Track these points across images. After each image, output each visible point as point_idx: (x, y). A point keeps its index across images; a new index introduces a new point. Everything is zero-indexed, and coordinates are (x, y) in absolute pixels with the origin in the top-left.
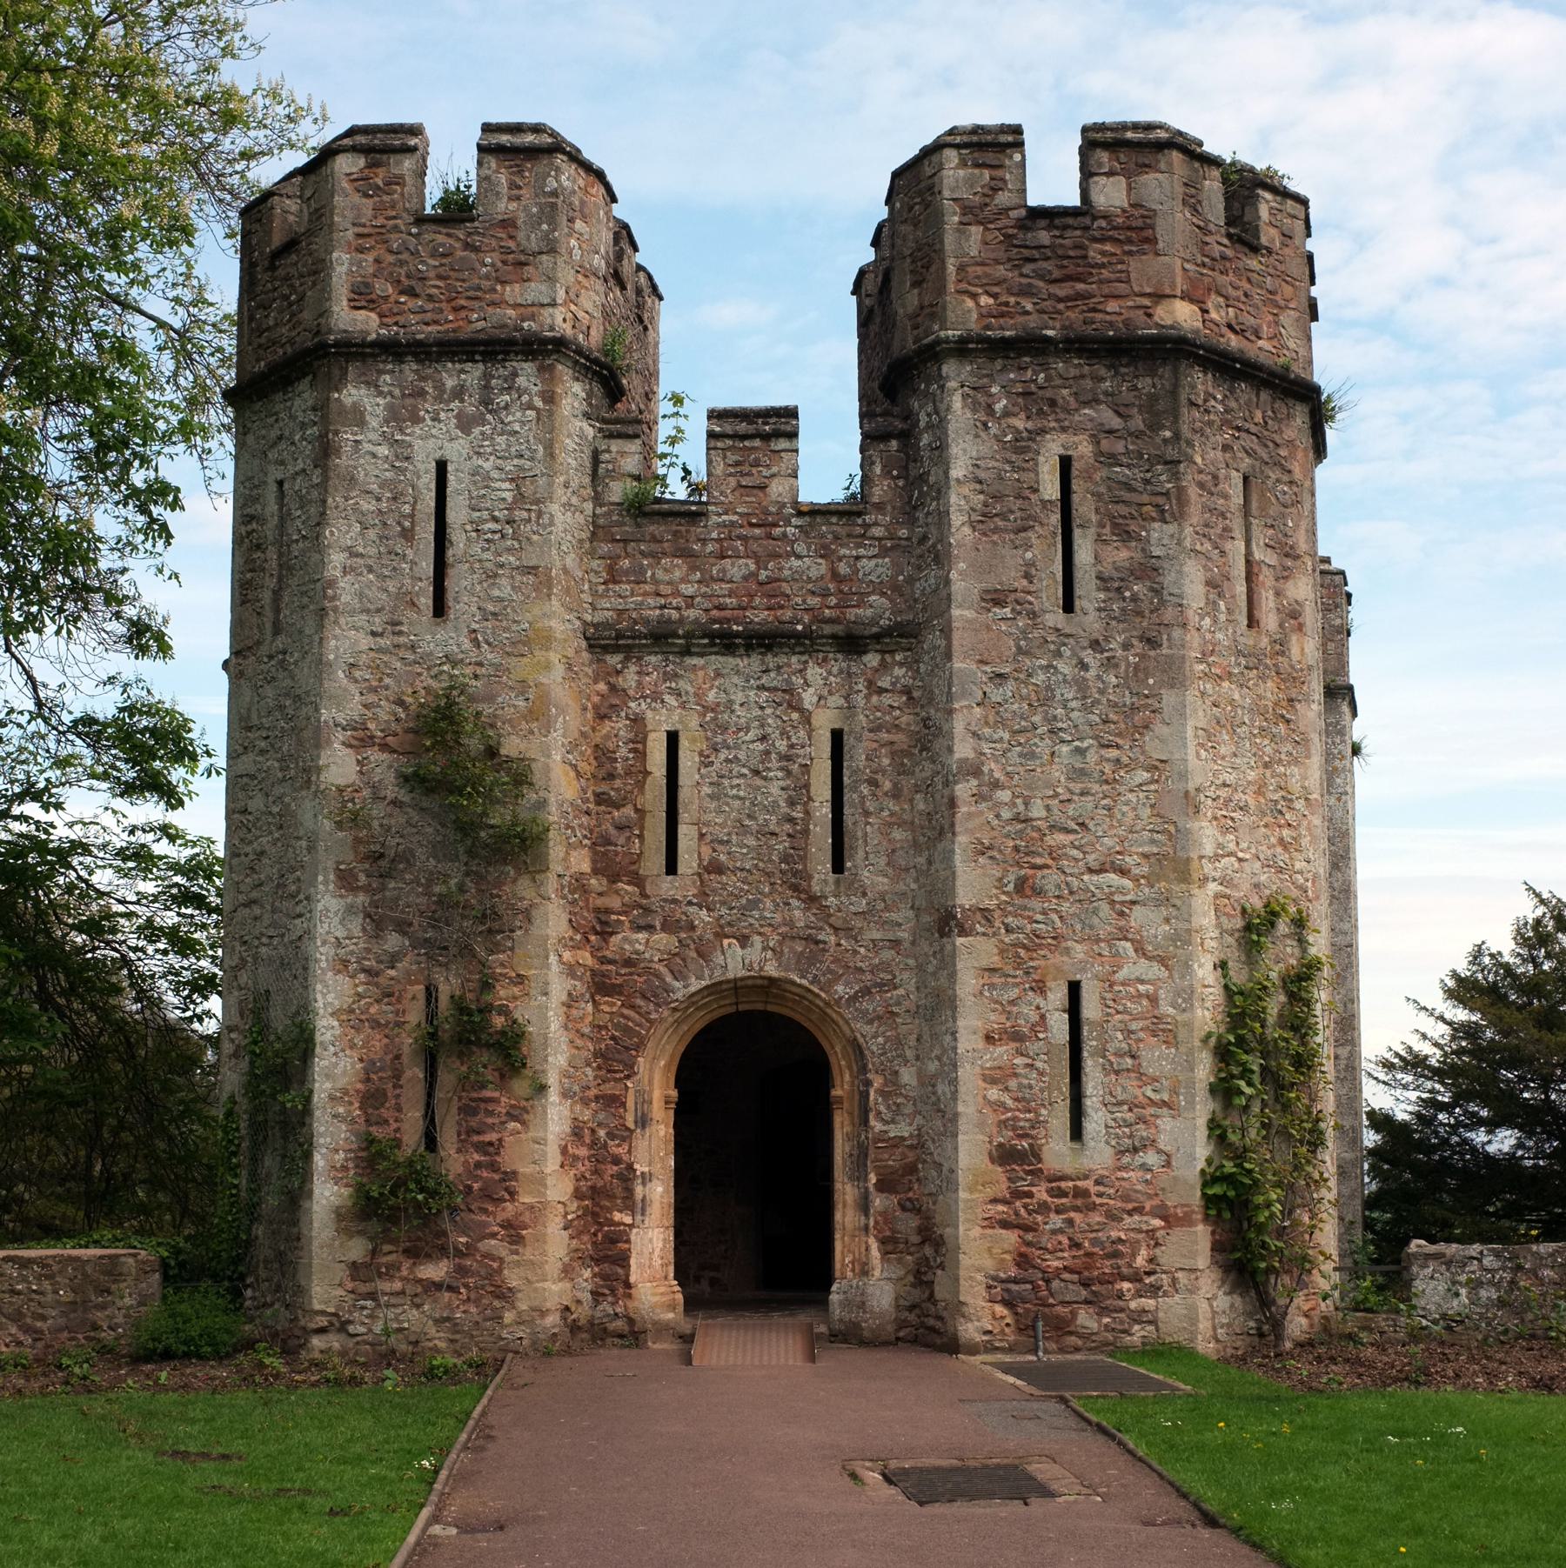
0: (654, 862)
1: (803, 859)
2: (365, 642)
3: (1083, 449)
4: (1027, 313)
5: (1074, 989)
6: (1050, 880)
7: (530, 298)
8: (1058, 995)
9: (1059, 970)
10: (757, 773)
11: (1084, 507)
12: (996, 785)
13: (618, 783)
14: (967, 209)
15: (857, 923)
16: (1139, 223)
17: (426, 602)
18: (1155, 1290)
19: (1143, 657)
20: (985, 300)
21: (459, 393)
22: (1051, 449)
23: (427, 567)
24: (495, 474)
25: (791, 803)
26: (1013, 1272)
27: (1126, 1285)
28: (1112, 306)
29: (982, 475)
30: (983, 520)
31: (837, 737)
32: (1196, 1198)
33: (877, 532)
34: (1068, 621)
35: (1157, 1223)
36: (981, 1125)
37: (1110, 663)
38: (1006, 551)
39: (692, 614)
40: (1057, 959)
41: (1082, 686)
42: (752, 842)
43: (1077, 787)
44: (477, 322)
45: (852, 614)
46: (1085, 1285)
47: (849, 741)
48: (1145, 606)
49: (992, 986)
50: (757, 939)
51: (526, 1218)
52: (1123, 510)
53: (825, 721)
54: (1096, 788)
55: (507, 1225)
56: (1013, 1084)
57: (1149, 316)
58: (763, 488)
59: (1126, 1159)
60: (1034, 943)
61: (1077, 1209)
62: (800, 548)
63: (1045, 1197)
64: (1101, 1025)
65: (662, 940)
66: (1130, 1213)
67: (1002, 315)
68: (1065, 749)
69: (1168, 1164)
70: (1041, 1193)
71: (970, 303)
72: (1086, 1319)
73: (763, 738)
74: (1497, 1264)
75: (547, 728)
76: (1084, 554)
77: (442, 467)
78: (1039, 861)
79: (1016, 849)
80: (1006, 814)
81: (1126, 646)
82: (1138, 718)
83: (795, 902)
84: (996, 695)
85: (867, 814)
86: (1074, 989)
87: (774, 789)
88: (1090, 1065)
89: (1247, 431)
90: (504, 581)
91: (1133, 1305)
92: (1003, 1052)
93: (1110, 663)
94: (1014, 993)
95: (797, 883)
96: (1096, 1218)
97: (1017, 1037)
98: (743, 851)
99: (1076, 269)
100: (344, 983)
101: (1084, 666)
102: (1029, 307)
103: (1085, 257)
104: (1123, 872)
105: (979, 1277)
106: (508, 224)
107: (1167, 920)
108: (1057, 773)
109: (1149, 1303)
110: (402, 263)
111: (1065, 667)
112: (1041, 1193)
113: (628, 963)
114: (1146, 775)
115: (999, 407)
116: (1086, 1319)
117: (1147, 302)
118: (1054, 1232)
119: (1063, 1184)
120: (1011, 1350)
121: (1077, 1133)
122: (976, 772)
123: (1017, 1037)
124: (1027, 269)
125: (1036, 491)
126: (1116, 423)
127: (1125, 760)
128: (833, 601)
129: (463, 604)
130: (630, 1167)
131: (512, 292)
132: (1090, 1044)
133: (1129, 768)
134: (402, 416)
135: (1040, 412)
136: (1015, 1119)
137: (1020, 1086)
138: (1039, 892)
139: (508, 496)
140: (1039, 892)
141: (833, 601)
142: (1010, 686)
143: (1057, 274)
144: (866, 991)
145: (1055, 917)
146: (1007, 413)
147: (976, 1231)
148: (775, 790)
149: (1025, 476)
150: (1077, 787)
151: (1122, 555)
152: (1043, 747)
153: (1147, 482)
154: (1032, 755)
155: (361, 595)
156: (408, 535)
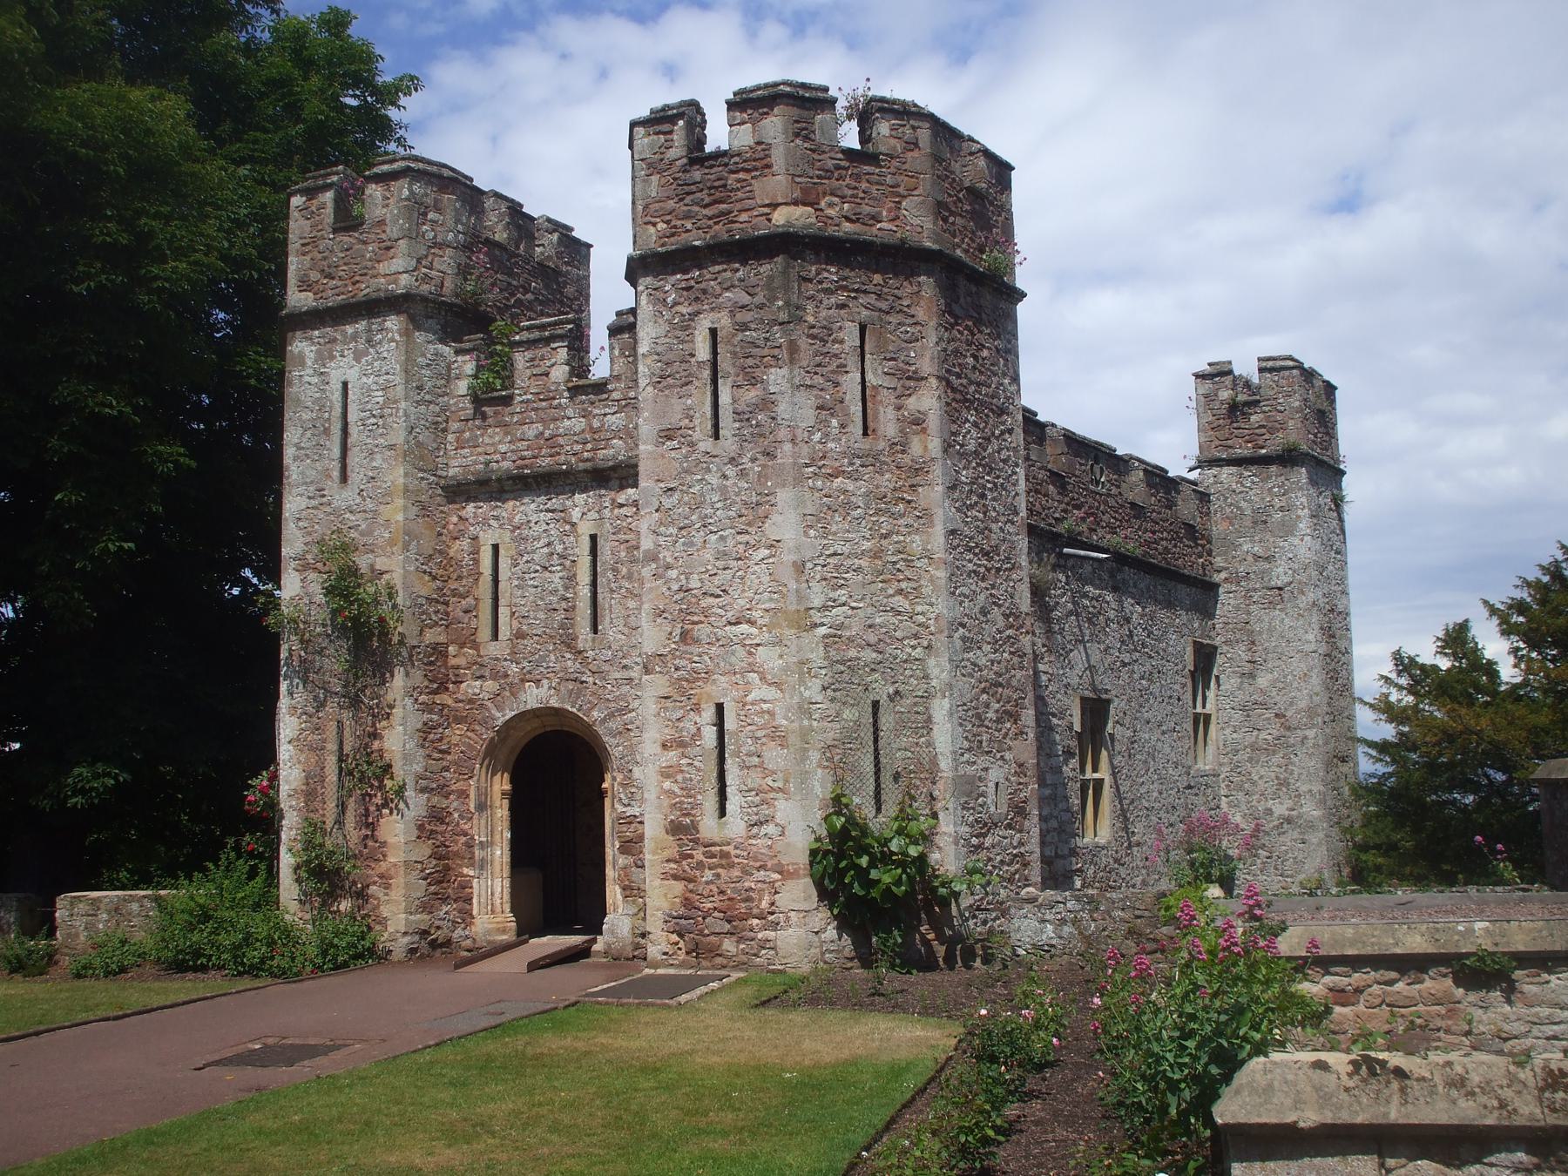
0: (485, 633)
1: (572, 625)
2: (304, 502)
3: (724, 321)
4: (688, 231)
5: (720, 708)
6: (702, 631)
7: (393, 269)
8: (709, 714)
9: (709, 695)
10: (546, 568)
11: (725, 363)
12: (668, 567)
13: (464, 582)
14: (650, 165)
15: (606, 667)
16: (762, 155)
17: (336, 474)
18: (775, 926)
19: (764, 466)
20: (662, 226)
21: (355, 337)
22: (704, 324)
23: (336, 452)
24: (374, 387)
25: (566, 588)
26: (682, 911)
27: (755, 921)
28: (744, 217)
29: (659, 349)
30: (660, 380)
31: (593, 538)
32: (803, 859)
33: (615, 395)
34: (715, 446)
35: (777, 876)
36: (660, 807)
37: (742, 474)
38: (674, 400)
39: (506, 464)
40: (709, 688)
41: (723, 490)
42: (542, 615)
43: (720, 564)
44: (365, 289)
45: (601, 453)
46: (729, 922)
47: (600, 542)
48: (766, 430)
49: (666, 709)
50: (545, 682)
51: (392, 872)
52: (750, 362)
53: (585, 529)
54: (733, 563)
55: (382, 876)
56: (679, 777)
57: (769, 220)
58: (547, 375)
59: (755, 830)
60: (694, 678)
61: (722, 866)
62: (570, 412)
63: (701, 857)
64: (735, 734)
65: (491, 686)
66: (758, 869)
67: (673, 235)
68: (713, 537)
69: (782, 834)
70: (699, 855)
71: (652, 230)
72: (729, 945)
73: (549, 545)
74: (1079, 907)
75: (931, 524)
76: (725, 397)
77: (345, 384)
78: (695, 618)
79: (681, 610)
80: (675, 587)
81: (753, 460)
82: (761, 511)
83: (568, 656)
84: (668, 502)
85: (612, 591)
86: (720, 708)
87: (556, 578)
88: (731, 765)
89: (865, 292)
90: (378, 456)
91: (760, 936)
92: (672, 755)
93: (742, 474)
94: (679, 714)
95: (569, 643)
96: (736, 873)
97: (682, 744)
98: (538, 622)
99: (719, 193)
100: (295, 720)
101: (725, 477)
102: (689, 226)
103: (725, 186)
104: (751, 622)
105: (659, 914)
106: (382, 223)
107: (781, 656)
108: (708, 555)
109: (771, 934)
110: (325, 258)
111: (714, 480)
112: (699, 855)
113: (471, 701)
114: (767, 552)
115: (669, 300)
116: (729, 945)
117: (766, 210)
118: (707, 883)
119: (713, 849)
120: (682, 965)
121: (722, 812)
122: (655, 559)
123: (682, 744)
124: (688, 200)
125: (693, 355)
126: (746, 299)
127: (753, 542)
128: (589, 446)
129: (355, 477)
130: (472, 838)
131: (382, 268)
132: (729, 748)
133: (755, 547)
134: (323, 358)
135: (697, 299)
136: (681, 803)
137: (685, 779)
138: (697, 641)
139: (380, 400)
140: (697, 641)
141: (589, 446)
142: (677, 496)
143: (707, 200)
144: (612, 715)
145: (706, 658)
146: (676, 304)
147: (658, 882)
148: (556, 579)
149: (686, 346)
150: (720, 564)
151: (752, 395)
152: (698, 538)
153: (767, 339)
154: (692, 544)
155: (303, 473)
156: (327, 431)
